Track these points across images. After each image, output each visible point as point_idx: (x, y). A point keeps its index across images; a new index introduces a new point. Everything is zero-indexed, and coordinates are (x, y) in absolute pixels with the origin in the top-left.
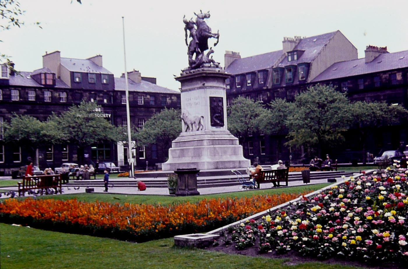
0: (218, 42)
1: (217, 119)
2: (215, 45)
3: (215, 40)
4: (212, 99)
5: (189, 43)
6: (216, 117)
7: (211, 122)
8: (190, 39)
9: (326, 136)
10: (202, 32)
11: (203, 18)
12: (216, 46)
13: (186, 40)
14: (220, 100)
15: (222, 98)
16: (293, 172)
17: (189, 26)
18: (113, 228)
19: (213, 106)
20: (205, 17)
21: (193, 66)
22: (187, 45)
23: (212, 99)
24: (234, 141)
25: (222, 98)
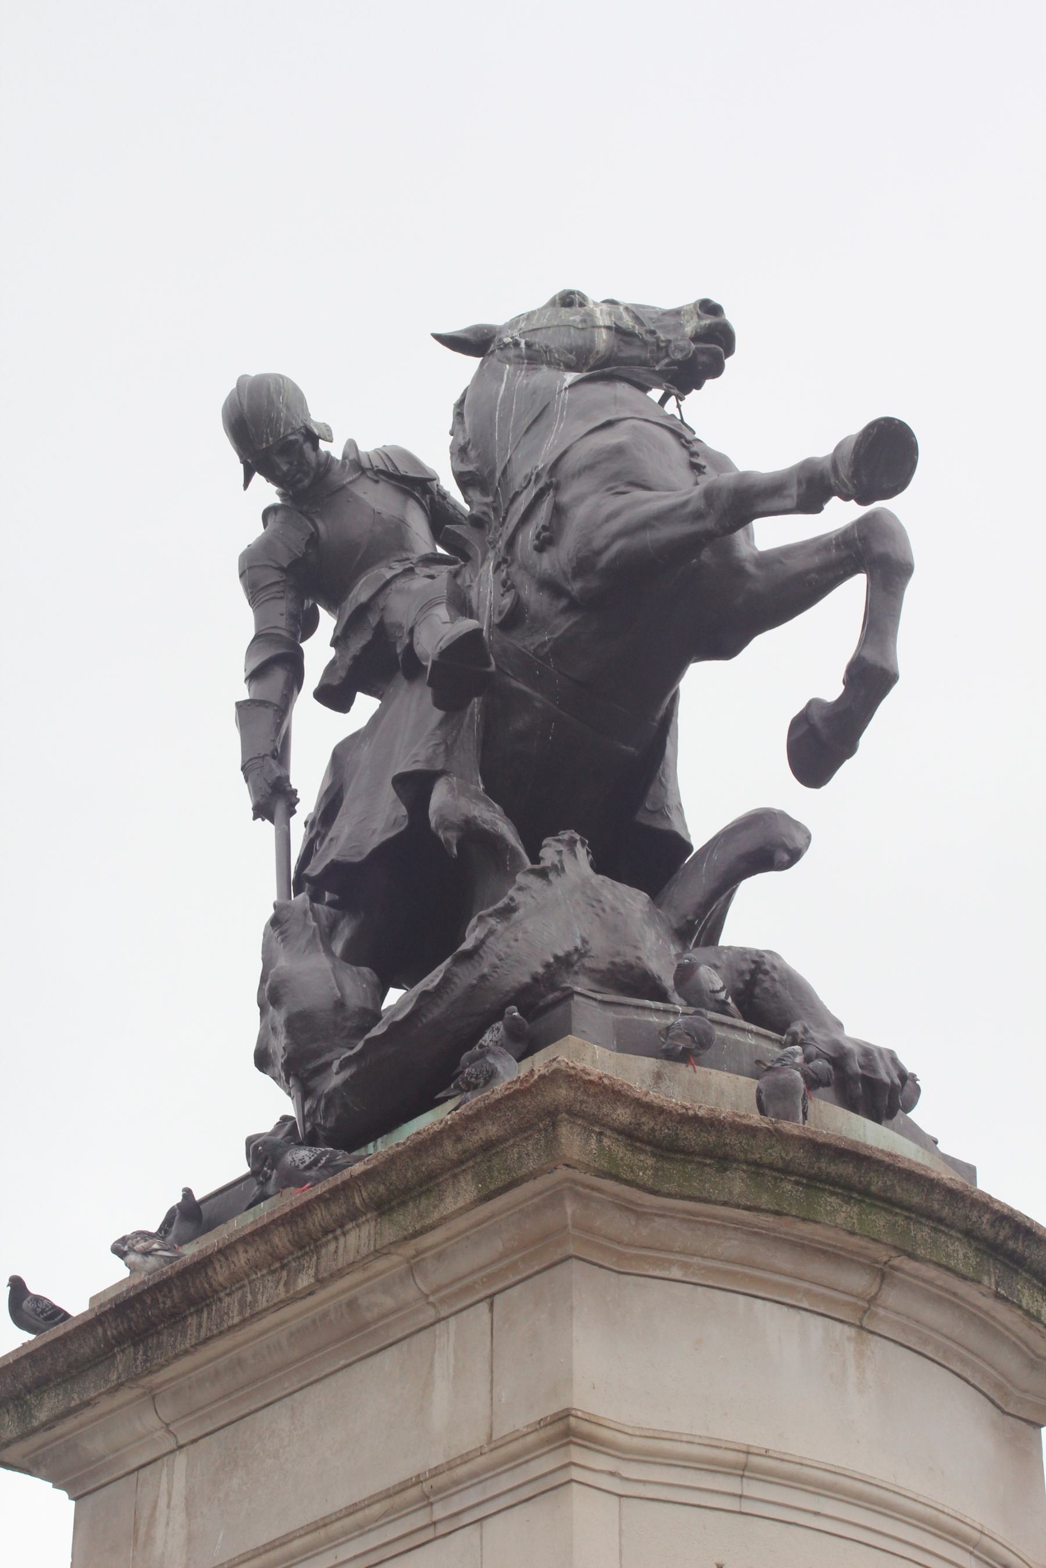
0: (869, 680)
5: (308, 776)
8: (316, 734)
22: (272, 798)
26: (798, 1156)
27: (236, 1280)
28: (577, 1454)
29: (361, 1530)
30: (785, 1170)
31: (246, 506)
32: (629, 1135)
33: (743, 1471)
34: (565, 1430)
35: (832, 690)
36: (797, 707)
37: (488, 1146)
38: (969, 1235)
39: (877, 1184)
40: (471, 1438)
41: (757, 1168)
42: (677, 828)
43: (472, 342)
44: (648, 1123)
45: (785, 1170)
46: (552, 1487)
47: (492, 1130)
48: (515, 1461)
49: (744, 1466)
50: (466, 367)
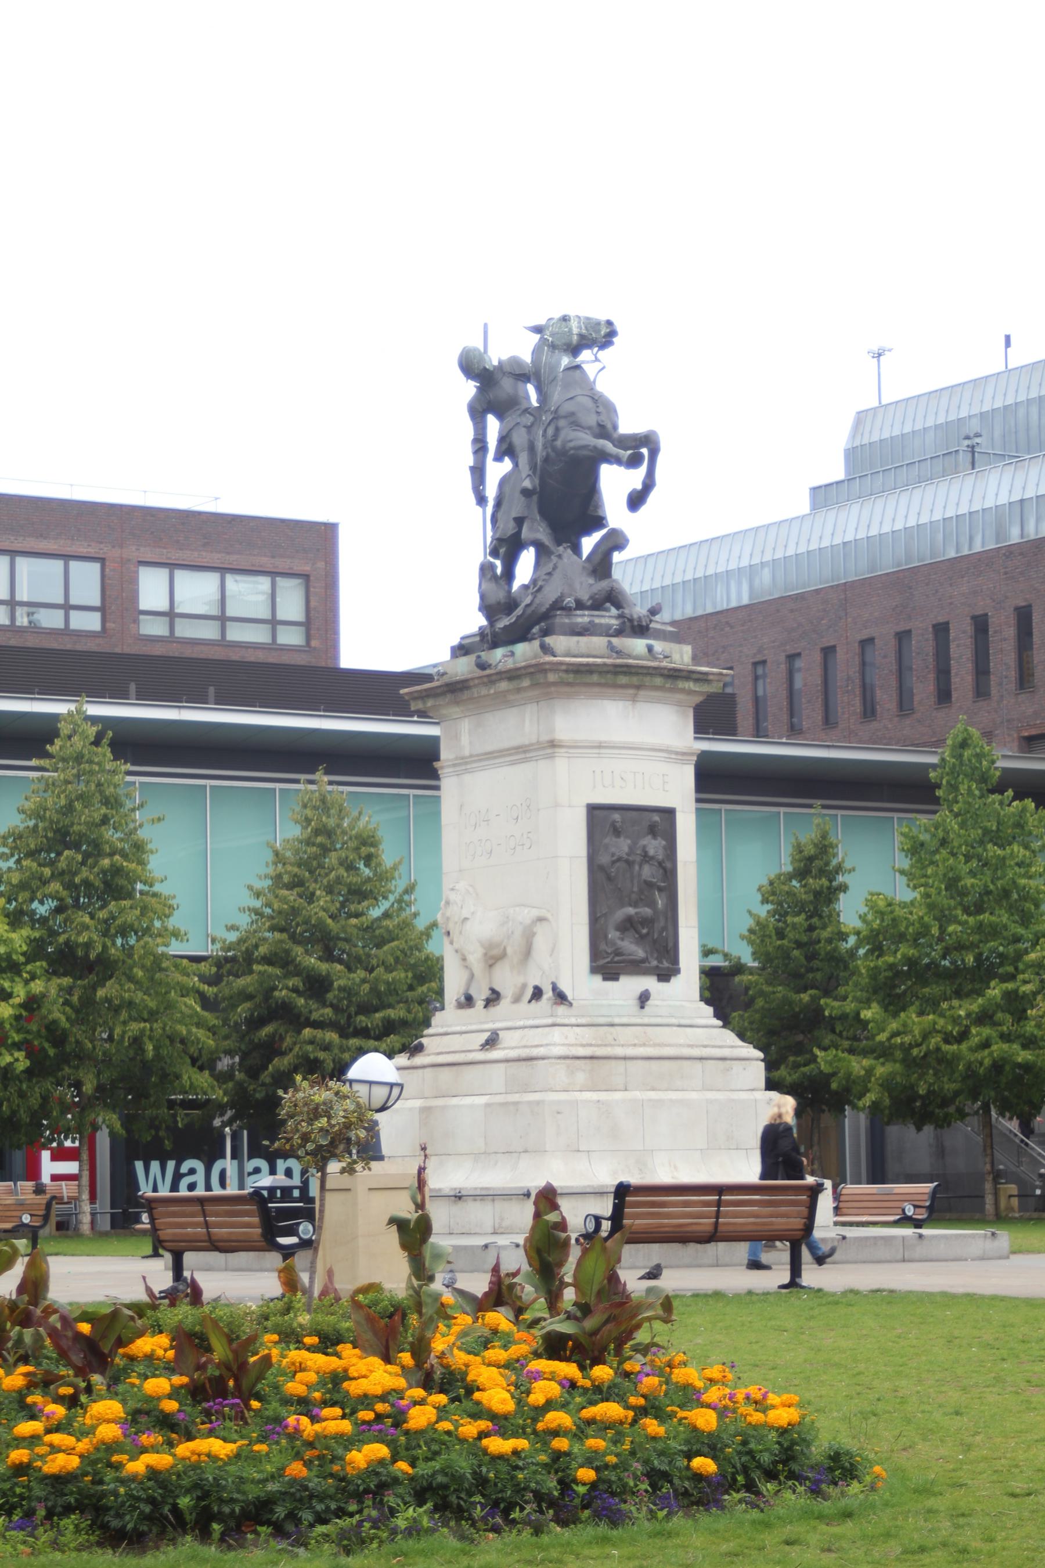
0: (648, 485)
1: (630, 924)
2: (636, 500)
3: (635, 478)
4: (602, 820)
5: (491, 491)
6: (628, 925)
7: (595, 953)
8: (497, 470)
9: (937, 1111)
10: (557, 430)
11: (575, 350)
12: (644, 509)
13: (478, 473)
14: (662, 821)
15: (669, 814)
16: (948, 1299)
17: (493, 388)
18: (222, 1540)
19: (604, 859)
20: (585, 342)
21: (504, 622)
22: (481, 500)
23: (602, 820)
24: (503, 1091)
25: (669, 814)
26: (611, 668)
27: (475, 686)
28: (557, 750)
29: (510, 755)
30: (608, 672)
31: (469, 389)
32: (566, 671)
33: (599, 747)
34: (553, 744)
35: (639, 487)
36: (630, 490)
37: (532, 673)
38: (662, 675)
39: (633, 670)
40: (534, 741)
41: (600, 673)
42: (601, 514)
43: (538, 330)
44: (571, 668)
45: (608, 672)
46: (551, 757)
47: (532, 670)
48: (544, 748)
49: (600, 746)
50: (537, 337)
